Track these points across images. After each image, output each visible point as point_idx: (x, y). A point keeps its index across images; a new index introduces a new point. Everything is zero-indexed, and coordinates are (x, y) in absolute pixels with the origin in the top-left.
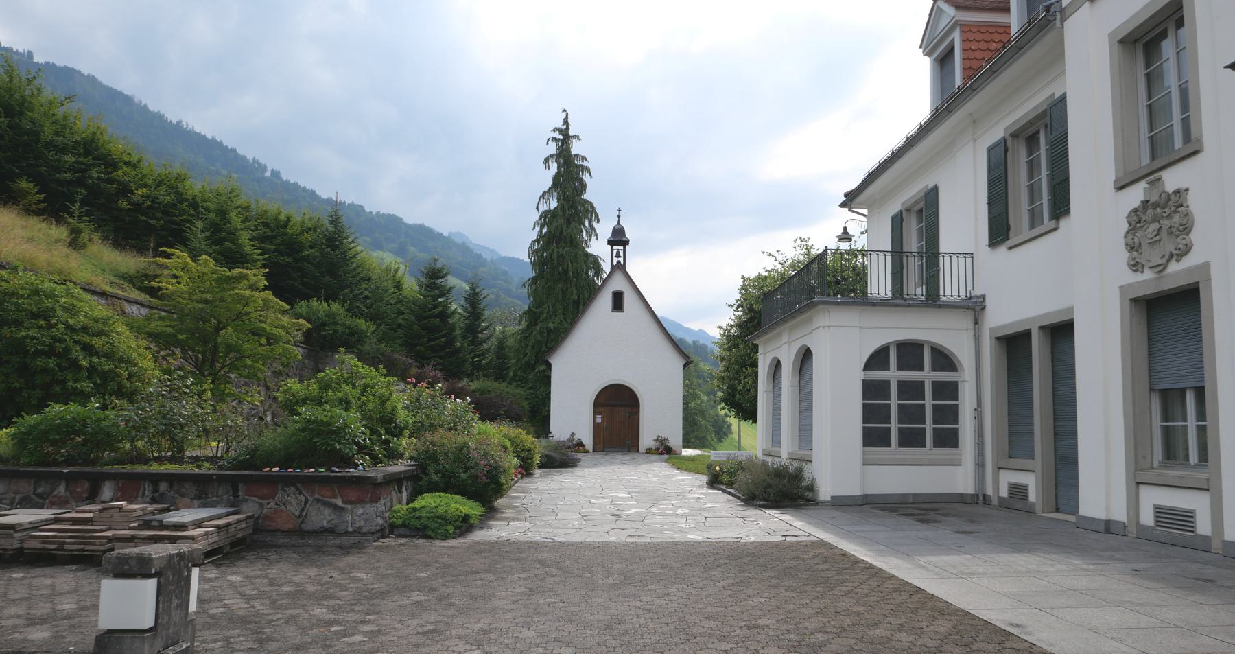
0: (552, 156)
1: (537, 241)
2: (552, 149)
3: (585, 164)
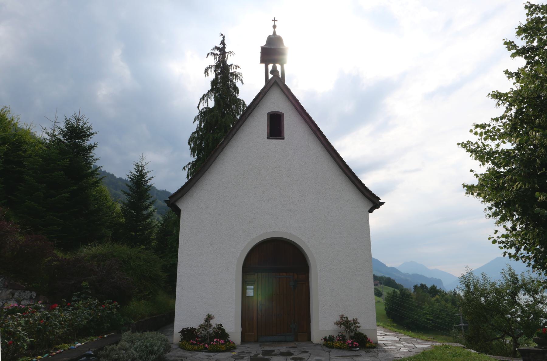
0: (211, 67)
1: (197, 132)
2: (212, 61)
3: (238, 71)
